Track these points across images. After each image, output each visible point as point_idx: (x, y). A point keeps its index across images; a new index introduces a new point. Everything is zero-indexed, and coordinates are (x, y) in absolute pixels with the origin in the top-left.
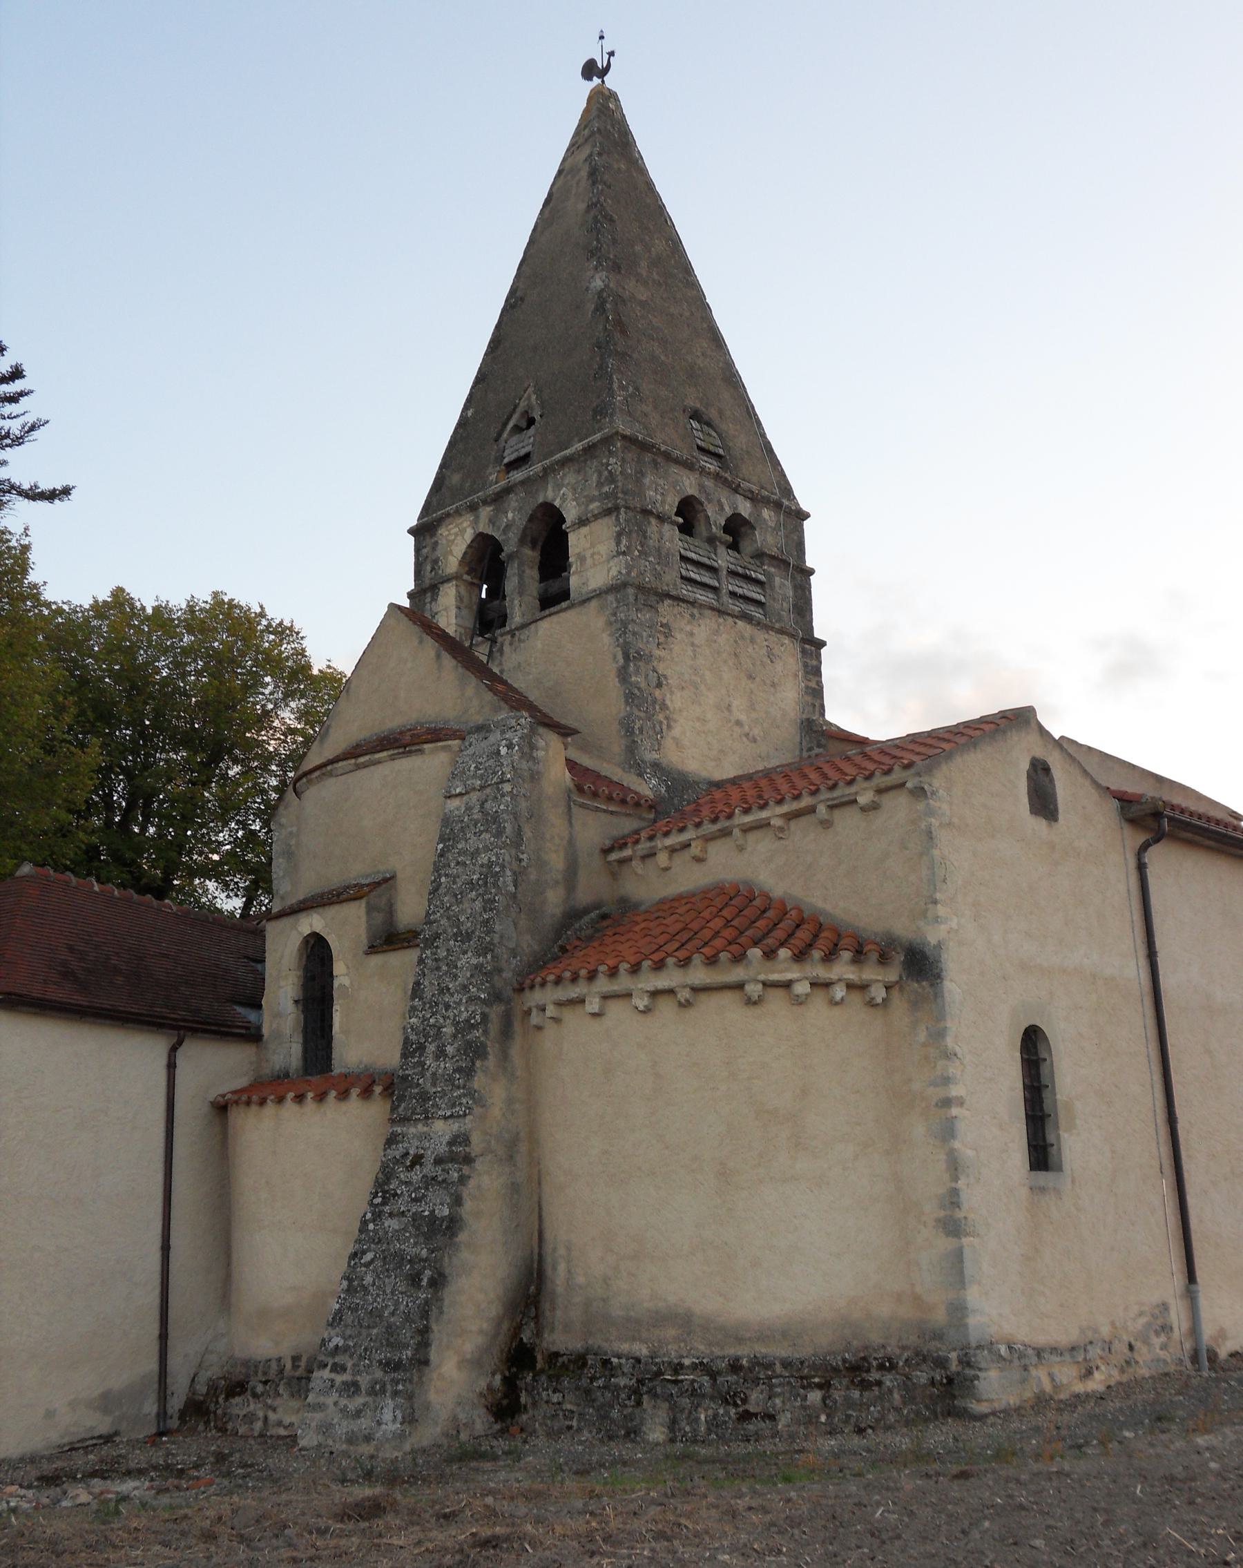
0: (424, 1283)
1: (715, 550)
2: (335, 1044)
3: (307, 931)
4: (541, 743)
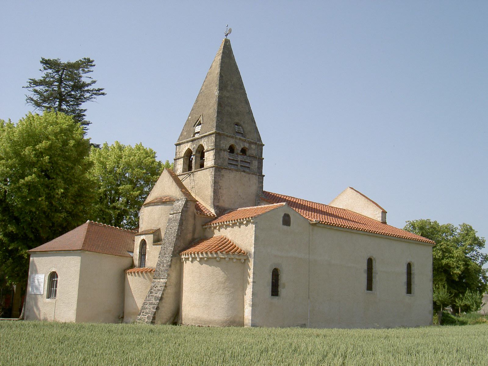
0: (155, 309)
1: (238, 156)
2: (146, 262)
3: (142, 239)
4: (189, 204)
